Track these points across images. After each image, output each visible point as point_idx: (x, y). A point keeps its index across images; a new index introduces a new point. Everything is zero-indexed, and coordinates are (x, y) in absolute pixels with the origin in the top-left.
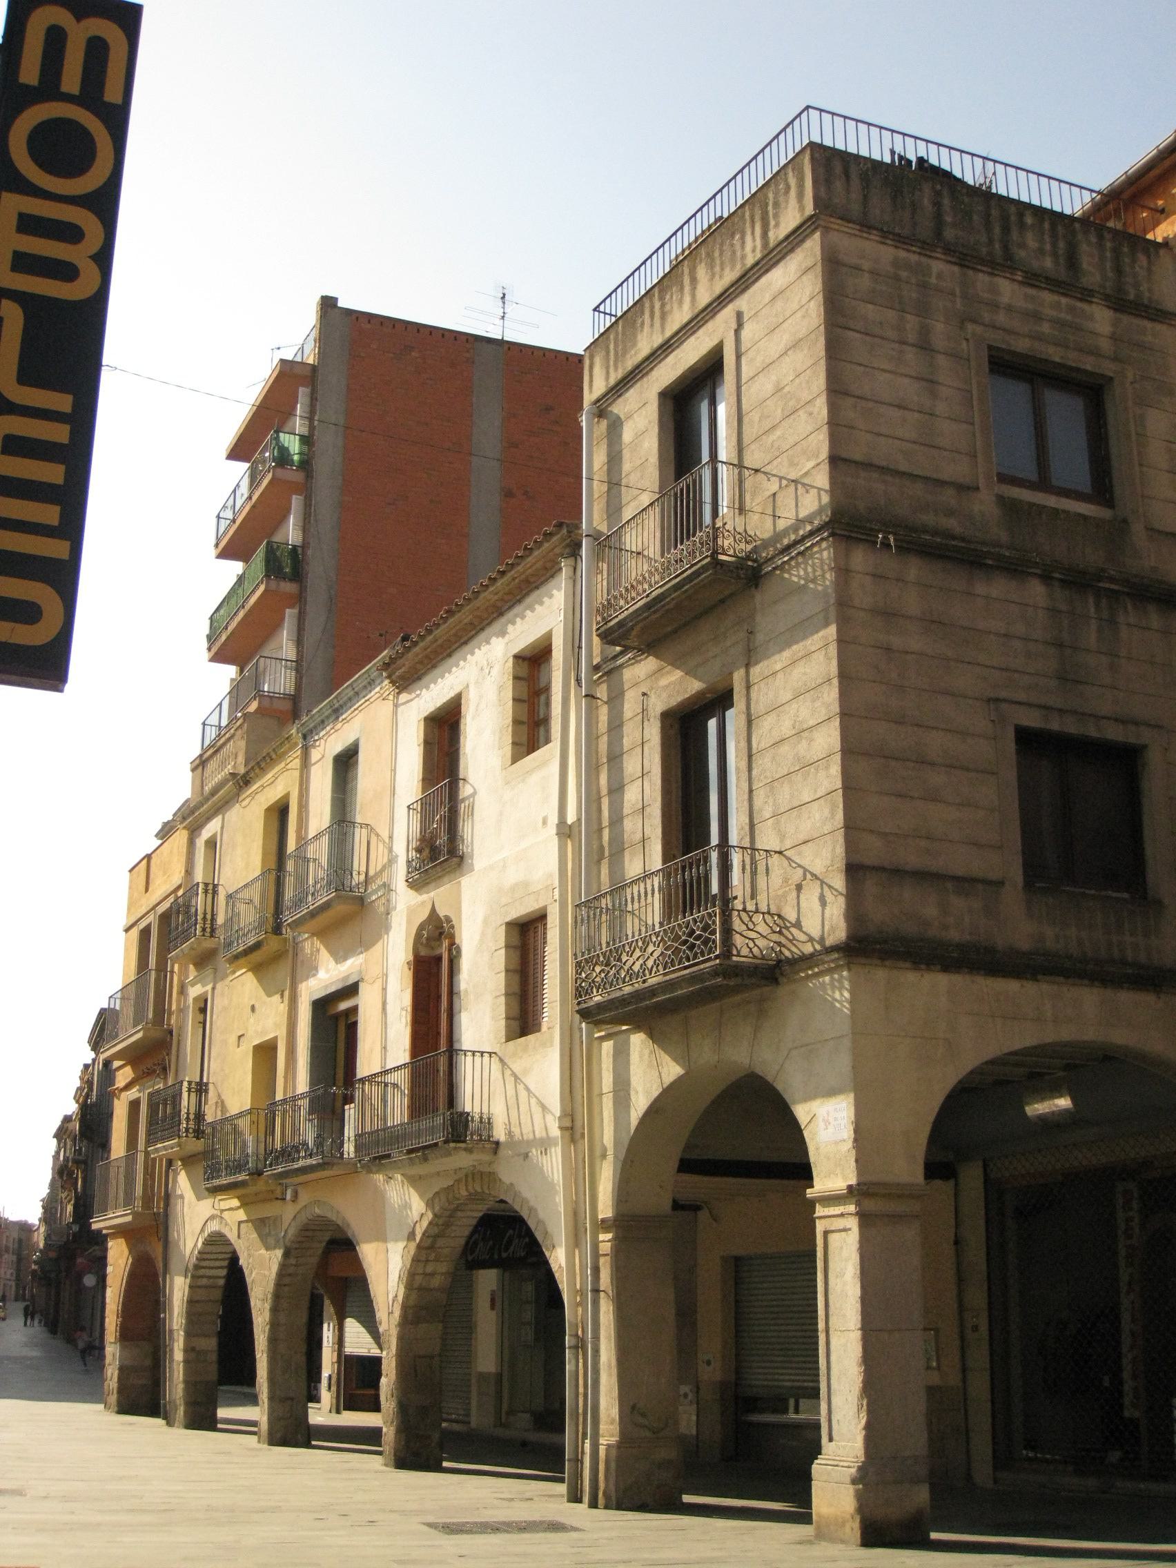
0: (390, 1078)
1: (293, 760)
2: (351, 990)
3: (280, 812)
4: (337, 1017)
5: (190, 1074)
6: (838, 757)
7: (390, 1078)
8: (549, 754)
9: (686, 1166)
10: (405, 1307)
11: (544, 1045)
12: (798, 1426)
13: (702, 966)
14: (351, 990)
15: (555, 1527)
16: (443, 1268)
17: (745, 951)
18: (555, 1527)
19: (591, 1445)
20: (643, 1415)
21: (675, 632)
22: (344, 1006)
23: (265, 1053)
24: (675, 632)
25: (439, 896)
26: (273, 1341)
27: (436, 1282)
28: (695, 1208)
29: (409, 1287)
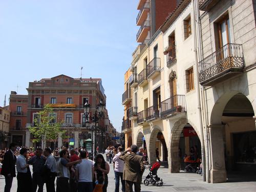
0: (166, 102)
1: (147, 50)
2: (159, 88)
3: (146, 60)
4: (157, 94)
5: (134, 105)
6: (254, 21)
7: (166, 102)
8: (191, 37)
9: (224, 114)
10: (171, 144)
11: (194, 93)
12: (215, 169)
13: (211, 172)
14: (159, 88)
15: (201, 188)
16: (178, 136)
17: (236, 66)
18: (201, 188)
19: (163, 147)
20: (218, 164)
21: (215, 5)
22: (158, 91)
23: (146, 101)
24: (215, 5)
25: (173, 68)
26: (150, 150)
27: (177, 139)
28: (225, 124)
29: (172, 140)
